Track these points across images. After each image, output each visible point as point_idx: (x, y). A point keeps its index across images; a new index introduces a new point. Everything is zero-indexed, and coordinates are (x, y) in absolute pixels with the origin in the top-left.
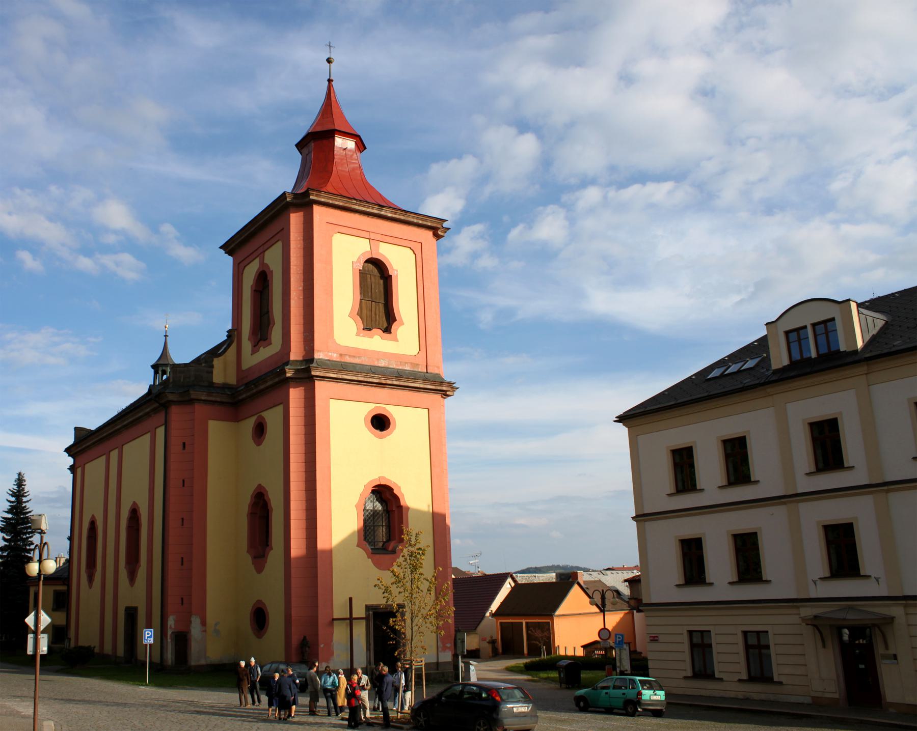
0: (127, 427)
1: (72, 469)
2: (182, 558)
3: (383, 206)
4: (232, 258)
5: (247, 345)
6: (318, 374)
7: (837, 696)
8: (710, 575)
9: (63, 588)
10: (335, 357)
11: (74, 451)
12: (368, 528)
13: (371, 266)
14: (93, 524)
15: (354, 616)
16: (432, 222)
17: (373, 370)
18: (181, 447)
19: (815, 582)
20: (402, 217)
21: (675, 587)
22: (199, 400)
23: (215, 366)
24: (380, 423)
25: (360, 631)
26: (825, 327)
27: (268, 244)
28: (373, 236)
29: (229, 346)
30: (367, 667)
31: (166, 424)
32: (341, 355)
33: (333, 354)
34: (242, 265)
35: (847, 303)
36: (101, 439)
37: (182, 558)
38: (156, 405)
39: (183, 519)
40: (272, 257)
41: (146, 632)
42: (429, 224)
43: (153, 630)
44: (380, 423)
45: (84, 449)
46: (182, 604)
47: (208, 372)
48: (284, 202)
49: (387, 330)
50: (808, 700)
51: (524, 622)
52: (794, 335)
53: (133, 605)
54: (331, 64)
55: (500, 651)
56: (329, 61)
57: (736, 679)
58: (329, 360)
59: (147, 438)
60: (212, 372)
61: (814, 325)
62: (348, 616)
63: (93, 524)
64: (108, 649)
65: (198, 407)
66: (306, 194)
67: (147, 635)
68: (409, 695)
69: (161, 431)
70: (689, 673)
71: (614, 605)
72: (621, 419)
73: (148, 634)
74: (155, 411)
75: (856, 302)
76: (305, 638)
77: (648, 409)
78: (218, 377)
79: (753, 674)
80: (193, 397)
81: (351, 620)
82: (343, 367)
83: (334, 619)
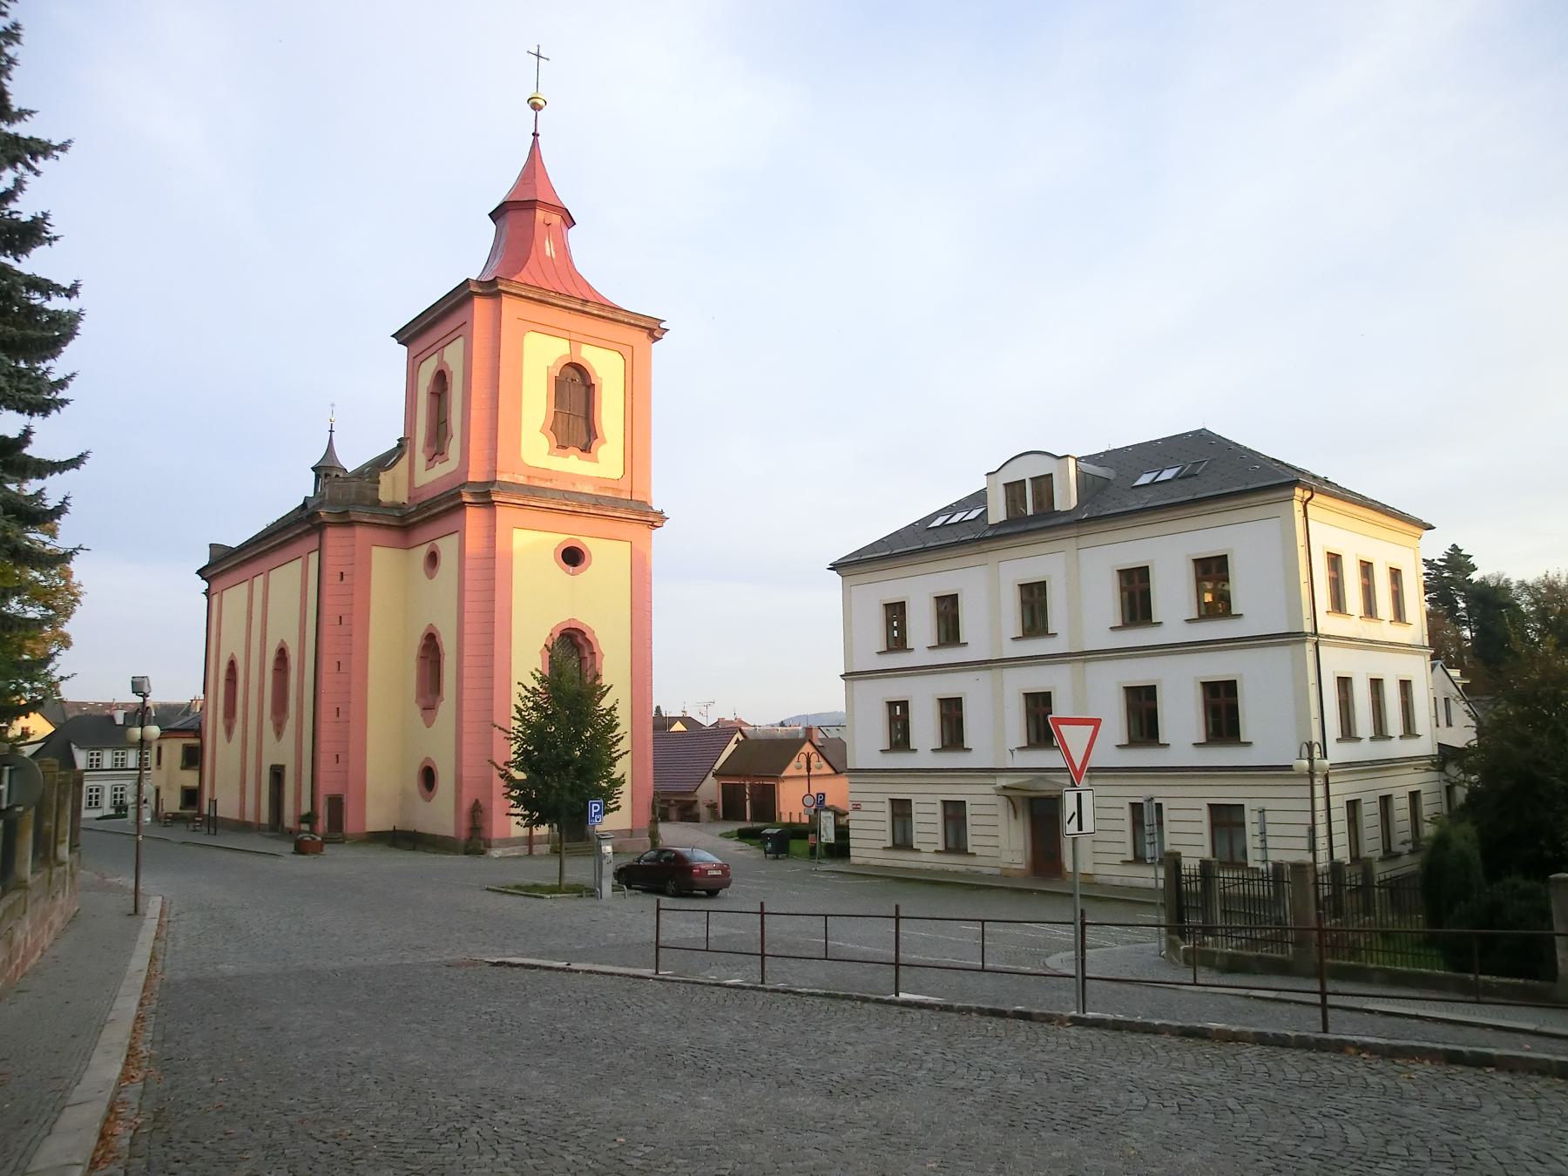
0: (273, 549)
1: (207, 593)
2: (338, 709)
3: (588, 301)
4: (406, 348)
5: (421, 459)
6: (499, 499)
7: (1023, 867)
8: (915, 739)
9: (196, 742)
10: (522, 480)
11: (209, 573)
13: (571, 372)
14: (232, 665)
16: (646, 321)
17: (567, 495)
18: (339, 577)
19: (1012, 751)
20: (610, 316)
21: (880, 753)
24: (573, 557)
26: (1044, 484)
27: (449, 339)
28: (574, 336)
29: (400, 457)
30: (549, 835)
31: (320, 550)
32: (529, 477)
34: (417, 363)
36: (244, 561)
37: (338, 709)
38: (309, 526)
40: (453, 355)
41: (593, 805)
44: (573, 557)
46: (338, 762)
48: (468, 291)
49: (586, 449)
50: (997, 871)
52: (1014, 490)
54: (539, 113)
55: (721, 816)
56: (536, 107)
57: (933, 850)
58: (514, 483)
59: (298, 563)
60: (377, 490)
63: (232, 665)
64: (250, 817)
65: (360, 531)
66: (493, 282)
67: (594, 811)
69: (314, 557)
70: (889, 844)
71: (798, 769)
72: (835, 567)
73: (596, 808)
74: (307, 533)
76: (477, 801)
77: (863, 558)
79: (897, 842)
80: (353, 518)
82: (531, 491)
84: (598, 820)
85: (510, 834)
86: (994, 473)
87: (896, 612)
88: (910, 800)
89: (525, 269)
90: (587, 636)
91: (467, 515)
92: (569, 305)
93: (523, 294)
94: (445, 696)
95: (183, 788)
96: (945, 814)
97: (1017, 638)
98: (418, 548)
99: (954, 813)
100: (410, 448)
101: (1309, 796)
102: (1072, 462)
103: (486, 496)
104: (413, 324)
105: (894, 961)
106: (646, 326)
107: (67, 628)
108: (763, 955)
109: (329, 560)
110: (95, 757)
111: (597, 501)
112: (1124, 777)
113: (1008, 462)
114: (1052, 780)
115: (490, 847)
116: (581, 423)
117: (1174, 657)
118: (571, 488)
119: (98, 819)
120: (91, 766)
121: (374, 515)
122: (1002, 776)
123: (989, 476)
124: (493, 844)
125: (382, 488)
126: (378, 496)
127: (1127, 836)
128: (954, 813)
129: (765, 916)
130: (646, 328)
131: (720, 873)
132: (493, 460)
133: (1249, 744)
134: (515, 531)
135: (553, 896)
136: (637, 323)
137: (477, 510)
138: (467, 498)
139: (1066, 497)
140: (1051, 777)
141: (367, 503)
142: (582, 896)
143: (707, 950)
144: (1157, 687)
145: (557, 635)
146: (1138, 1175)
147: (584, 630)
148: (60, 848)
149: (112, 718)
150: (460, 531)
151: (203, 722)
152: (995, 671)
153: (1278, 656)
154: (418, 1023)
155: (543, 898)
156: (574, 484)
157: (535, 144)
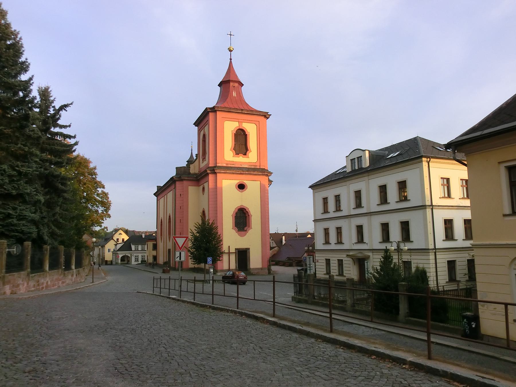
2: (181, 233)
6: (217, 171)
9: (155, 242)
10: (224, 165)
13: (240, 131)
15: (230, 252)
18: (180, 195)
20: (251, 113)
23: (191, 167)
24: (241, 187)
25: (233, 258)
28: (240, 121)
32: (227, 164)
37: (181, 233)
39: (180, 220)
41: (209, 259)
45: (170, 185)
49: (245, 154)
51: (15, 250)
53: (170, 248)
56: (231, 51)
60: (190, 170)
61: (358, 158)
63: (170, 217)
65: (185, 182)
67: (209, 260)
72: (310, 187)
73: (210, 259)
80: (182, 178)
81: (229, 253)
86: (348, 156)
87: (325, 200)
88: (343, 260)
89: (226, 101)
90: (246, 210)
91: (209, 176)
92: (237, 111)
93: (223, 110)
94: (252, 227)
95: (153, 256)
96: (339, 264)
99: (340, 263)
101: (397, 258)
102: (367, 152)
103: (214, 170)
105: (212, 294)
107: (110, 212)
108: (194, 293)
109: (177, 191)
112: (326, 252)
113: (353, 151)
115: (217, 272)
116: (244, 147)
117: (391, 214)
118: (240, 166)
120: (136, 249)
121: (188, 177)
123: (347, 157)
124: (218, 271)
125: (191, 169)
126: (190, 172)
127: (325, 267)
128: (340, 263)
129: (171, 280)
130: (264, 115)
131: (243, 278)
132: (216, 159)
133: (412, 242)
134: (223, 181)
136: (260, 114)
138: (209, 172)
139: (366, 163)
140: (363, 252)
143: (187, 292)
144: (409, 222)
145: (237, 210)
146: (1, 277)
147: (246, 209)
148: (72, 266)
149: (142, 236)
150: (208, 181)
151: (157, 238)
152: (350, 219)
153: (420, 212)
154: (357, 359)
156: (241, 165)
157: (231, 62)
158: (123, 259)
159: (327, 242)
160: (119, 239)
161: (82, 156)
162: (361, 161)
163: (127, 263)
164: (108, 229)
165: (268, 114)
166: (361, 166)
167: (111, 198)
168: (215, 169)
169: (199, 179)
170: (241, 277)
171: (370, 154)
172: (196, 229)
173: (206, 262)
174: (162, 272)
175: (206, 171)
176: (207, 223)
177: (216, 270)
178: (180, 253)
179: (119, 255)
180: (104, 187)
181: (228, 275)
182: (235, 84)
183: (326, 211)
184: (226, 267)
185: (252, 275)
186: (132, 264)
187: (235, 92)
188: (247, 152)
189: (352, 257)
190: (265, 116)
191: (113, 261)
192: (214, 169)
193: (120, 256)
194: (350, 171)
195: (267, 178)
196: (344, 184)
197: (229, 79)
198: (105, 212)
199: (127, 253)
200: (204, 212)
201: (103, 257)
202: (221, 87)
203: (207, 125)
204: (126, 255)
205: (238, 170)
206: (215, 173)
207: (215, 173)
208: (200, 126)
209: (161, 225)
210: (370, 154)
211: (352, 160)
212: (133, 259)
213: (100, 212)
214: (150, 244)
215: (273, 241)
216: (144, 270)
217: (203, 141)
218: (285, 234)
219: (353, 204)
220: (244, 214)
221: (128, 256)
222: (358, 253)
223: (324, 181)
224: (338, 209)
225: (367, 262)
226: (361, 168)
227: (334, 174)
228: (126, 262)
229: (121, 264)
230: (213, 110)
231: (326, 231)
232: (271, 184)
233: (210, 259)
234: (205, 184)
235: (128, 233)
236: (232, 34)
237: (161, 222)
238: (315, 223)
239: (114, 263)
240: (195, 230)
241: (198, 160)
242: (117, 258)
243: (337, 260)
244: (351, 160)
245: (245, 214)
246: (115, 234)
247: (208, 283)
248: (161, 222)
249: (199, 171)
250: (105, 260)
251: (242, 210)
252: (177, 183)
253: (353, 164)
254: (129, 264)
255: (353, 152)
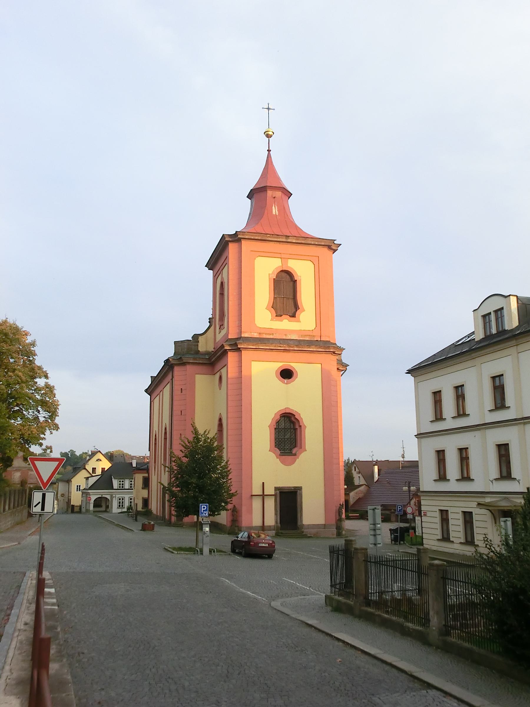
3: (289, 236)
4: (212, 271)
6: (242, 346)
9: (146, 475)
10: (256, 335)
11: (149, 391)
12: (280, 440)
13: (284, 275)
18: (180, 391)
20: (303, 242)
22: (189, 363)
23: (200, 341)
25: (271, 505)
28: (283, 256)
30: (274, 526)
32: (260, 333)
33: (254, 333)
34: (216, 276)
35: (509, 297)
41: (202, 506)
42: (323, 244)
43: (200, 504)
47: (195, 345)
49: (294, 316)
54: (270, 139)
56: (269, 136)
60: (198, 345)
61: (496, 311)
62: (261, 494)
65: (188, 367)
67: (202, 509)
68: (526, 565)
72: (409, 372)
73: (204, 508)
75: (517, 296)
78: (202, 348)
80: (184, 361)
81: (263, 496)
83: (252, 496)
84: (205, 514)
85: (261, 526)
87: (437, 395)
93: (252, 238)
94: (307, 447)
95: (143, 498)
97: (491, 410)
98: (216, 374)
99: (468, 517)
100: (214, 323)
104: (211, 259)
106: (325, 244)
110: (121, 483)
111: (299, 342)
114: (513, 500)
116: (291, 302)
118: (284, 337)
119: (119, 513)
120: (120, 487)
121: (194, 359)
122: (487, 497)
124: (242, 529)
125: (200, 344)
127: (438, 526)
128: (468, 517)
131: (267, 545)
134: (253, 362)
135: (178, 552)
137: (236, 353)
138: (227, 348)
141: (193, 353)
142: (195, 554)
151: (149, 467)
152: (482, 431)
155: (173, 553)
157: (269, 156)
158: (98, 503)
159: (442, 477)
160: (95, 468)
161: (12, 322)
162: (502, 316)
163: (106, 511)
164: (53, 449)
165: (335, 242)
166: (502, 328)
167: (59, 396)
168: (238, 342)
169: (214, 361)
170: (263, 543)
171: (519, 302)
172: (183, 449)
173: (197, 512)
174: (141, 529)
175: (222, 346)
176: (203, 439)
177: (238, 526)
178: (44, 496)
179: (91, 496)
180: (46, 377)
181: (241, 539)
182: (277, 192)
183: (439, 417)
184: (257, 522)
185: (306, 537)
186: (113, 512)
187: (276, 206)
188: (297, 311)
189: (490, 508)
190: (329, 247)
191: (83, 506)
192: (236, 343)
193: (93, 498)
194: (481, 338)
195: (334, 358)
196: (469, 363)
197: (265, 185)
198: (49, 420)
199: (105, 493)
200: (220, 420)
201: (69, 499)
202: (252, 199)
203: (227, 266)
204: (103, 496)
205: (281, 344)
206: (239, 350)
207: (239, 350)
208: (216, 270)
209: (155, 444)
210: (519, 302)
211: (486, 317)
212: (115, 504)
213: (42, 419)
214: (139, 478)
215: (360, 475)
216: (118, 525)
217: (220, 294)
218: (377, 463)
219: (489, 402)
220: (292, 425)
221: (107, 498)
222: (501, 500)
223: (434, 359)
224: (461, 413)
225: (505, 521)
226: (502, 332)
227: (455, 346)
228: (103, 509)
229: (94, 512)
230: (236, 238)
231: (441, 454)
232: (345, 371)
233: (204, 508)
234: (222, 370)
235: (114, 458)
236: (270, 107)
237: (156, 439)
238: (419, 439)
239: (83, 510)
240: (181, 450)
241: (212, 328)
242: (88, 501)
243: (461, 513)
244: (484, 316)
245: (293, 423)
246: (89, 460)
247: (197, 554)
248: (156, 439)
249: (214, 348)
250: (72, 504)
251: (288, 417)
252: (176, 369)
253: (488, 324)
254: (108, 512)
255: (484, 303)
